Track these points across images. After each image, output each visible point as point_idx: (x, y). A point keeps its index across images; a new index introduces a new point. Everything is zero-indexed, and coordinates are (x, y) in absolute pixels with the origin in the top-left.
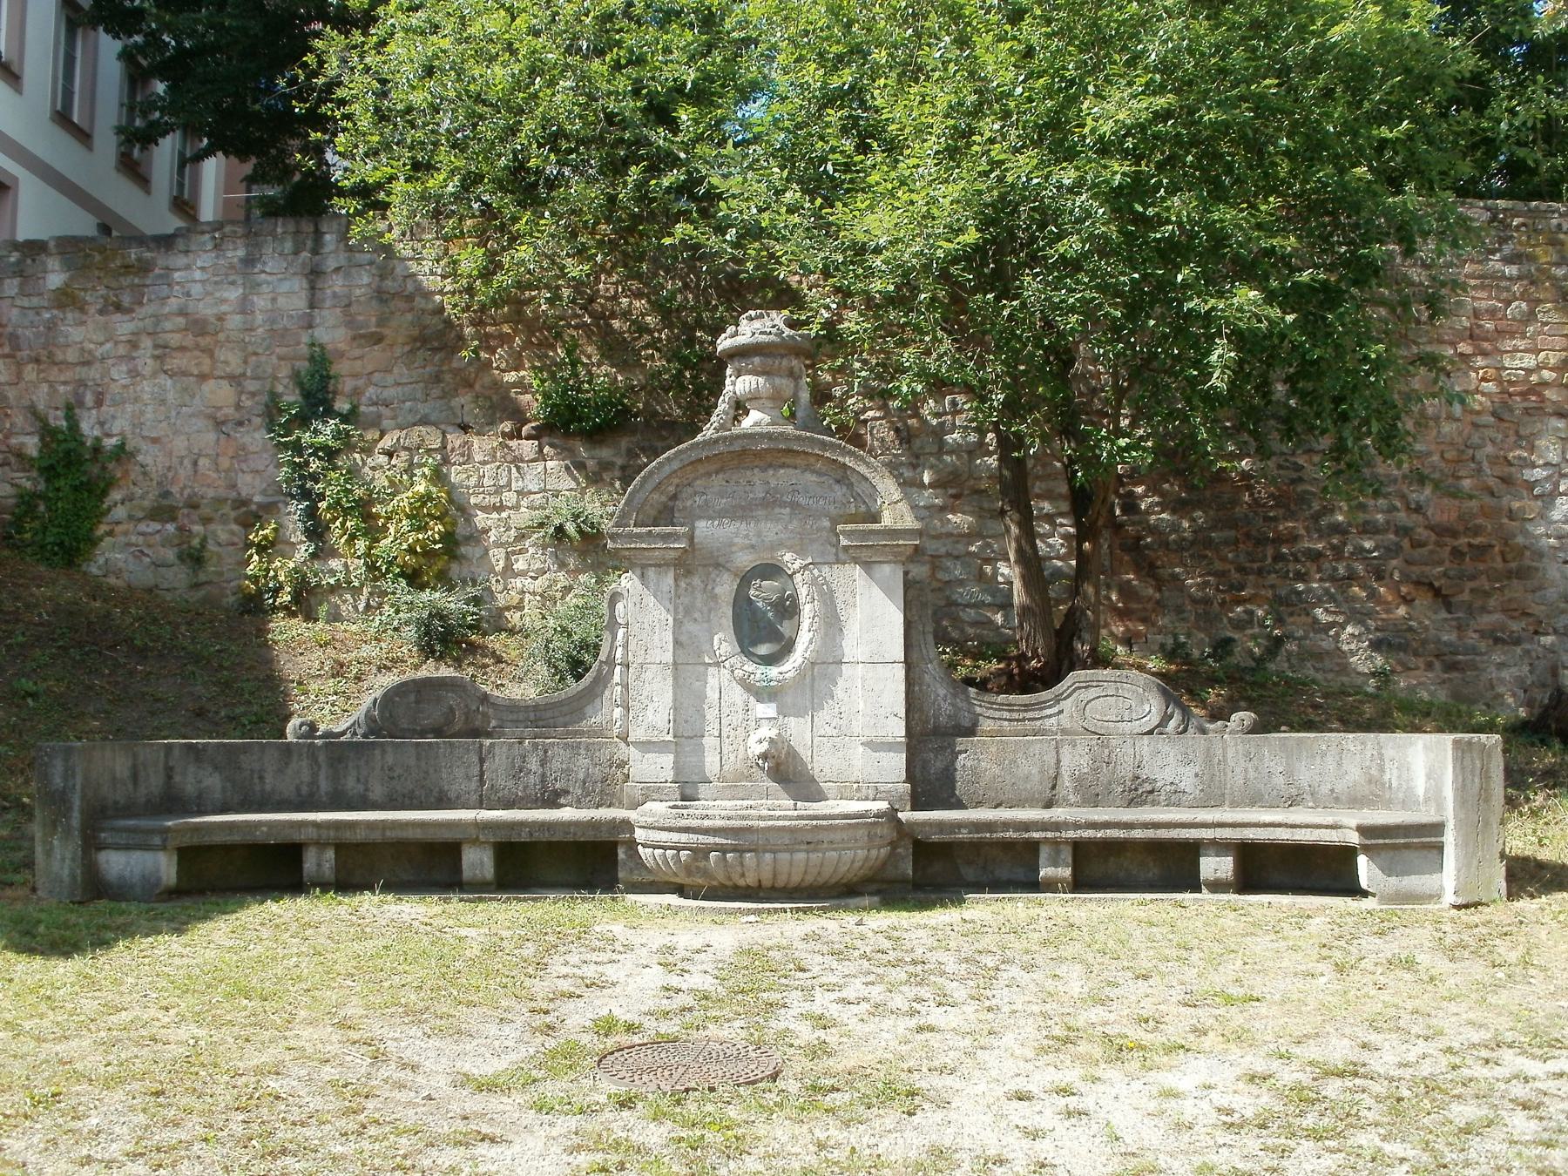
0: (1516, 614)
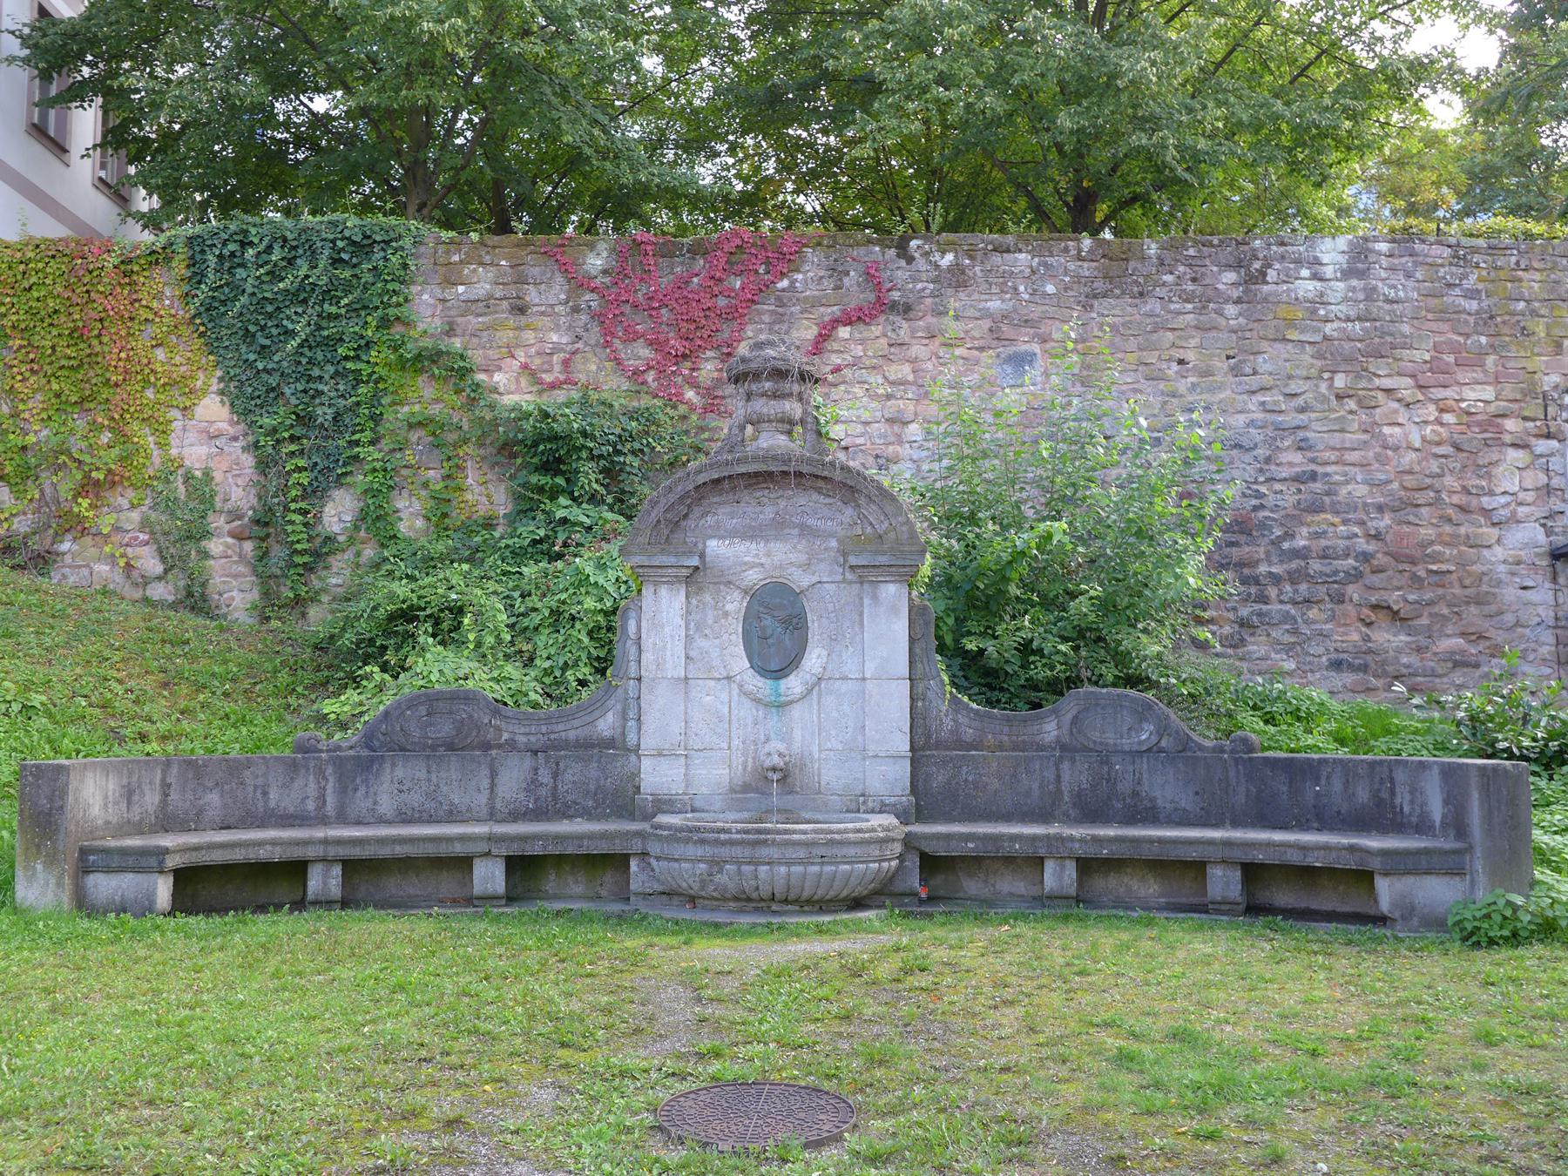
0: (1474, 637)
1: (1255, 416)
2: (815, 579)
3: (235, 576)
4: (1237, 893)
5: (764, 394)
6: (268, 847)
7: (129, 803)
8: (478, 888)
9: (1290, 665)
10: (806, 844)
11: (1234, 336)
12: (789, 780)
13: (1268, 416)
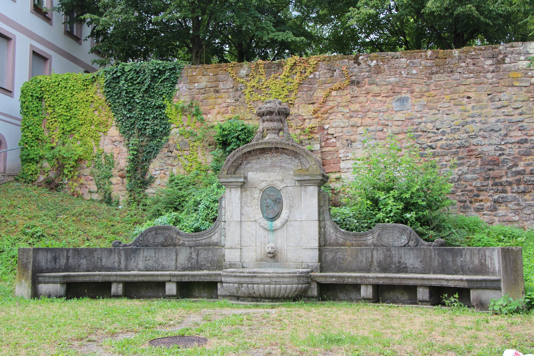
1: (500, 118)
2: (285, 185)
3: (121, 191)
4: (428, 298)
5: (267, 120)
6: (98, 277)
7: (55, 262)
8: (167, 293)
9: (517, 218)
10: (270, 277)
11: (491, 86)
12: (276, 257)
13: (506, 117)
